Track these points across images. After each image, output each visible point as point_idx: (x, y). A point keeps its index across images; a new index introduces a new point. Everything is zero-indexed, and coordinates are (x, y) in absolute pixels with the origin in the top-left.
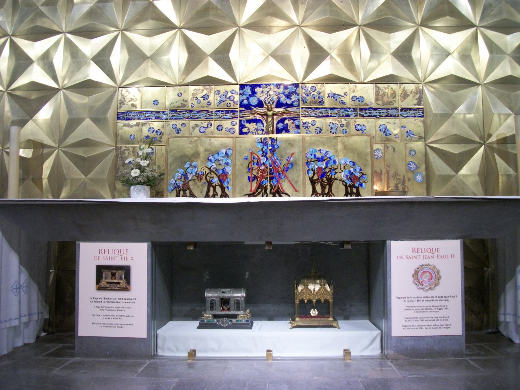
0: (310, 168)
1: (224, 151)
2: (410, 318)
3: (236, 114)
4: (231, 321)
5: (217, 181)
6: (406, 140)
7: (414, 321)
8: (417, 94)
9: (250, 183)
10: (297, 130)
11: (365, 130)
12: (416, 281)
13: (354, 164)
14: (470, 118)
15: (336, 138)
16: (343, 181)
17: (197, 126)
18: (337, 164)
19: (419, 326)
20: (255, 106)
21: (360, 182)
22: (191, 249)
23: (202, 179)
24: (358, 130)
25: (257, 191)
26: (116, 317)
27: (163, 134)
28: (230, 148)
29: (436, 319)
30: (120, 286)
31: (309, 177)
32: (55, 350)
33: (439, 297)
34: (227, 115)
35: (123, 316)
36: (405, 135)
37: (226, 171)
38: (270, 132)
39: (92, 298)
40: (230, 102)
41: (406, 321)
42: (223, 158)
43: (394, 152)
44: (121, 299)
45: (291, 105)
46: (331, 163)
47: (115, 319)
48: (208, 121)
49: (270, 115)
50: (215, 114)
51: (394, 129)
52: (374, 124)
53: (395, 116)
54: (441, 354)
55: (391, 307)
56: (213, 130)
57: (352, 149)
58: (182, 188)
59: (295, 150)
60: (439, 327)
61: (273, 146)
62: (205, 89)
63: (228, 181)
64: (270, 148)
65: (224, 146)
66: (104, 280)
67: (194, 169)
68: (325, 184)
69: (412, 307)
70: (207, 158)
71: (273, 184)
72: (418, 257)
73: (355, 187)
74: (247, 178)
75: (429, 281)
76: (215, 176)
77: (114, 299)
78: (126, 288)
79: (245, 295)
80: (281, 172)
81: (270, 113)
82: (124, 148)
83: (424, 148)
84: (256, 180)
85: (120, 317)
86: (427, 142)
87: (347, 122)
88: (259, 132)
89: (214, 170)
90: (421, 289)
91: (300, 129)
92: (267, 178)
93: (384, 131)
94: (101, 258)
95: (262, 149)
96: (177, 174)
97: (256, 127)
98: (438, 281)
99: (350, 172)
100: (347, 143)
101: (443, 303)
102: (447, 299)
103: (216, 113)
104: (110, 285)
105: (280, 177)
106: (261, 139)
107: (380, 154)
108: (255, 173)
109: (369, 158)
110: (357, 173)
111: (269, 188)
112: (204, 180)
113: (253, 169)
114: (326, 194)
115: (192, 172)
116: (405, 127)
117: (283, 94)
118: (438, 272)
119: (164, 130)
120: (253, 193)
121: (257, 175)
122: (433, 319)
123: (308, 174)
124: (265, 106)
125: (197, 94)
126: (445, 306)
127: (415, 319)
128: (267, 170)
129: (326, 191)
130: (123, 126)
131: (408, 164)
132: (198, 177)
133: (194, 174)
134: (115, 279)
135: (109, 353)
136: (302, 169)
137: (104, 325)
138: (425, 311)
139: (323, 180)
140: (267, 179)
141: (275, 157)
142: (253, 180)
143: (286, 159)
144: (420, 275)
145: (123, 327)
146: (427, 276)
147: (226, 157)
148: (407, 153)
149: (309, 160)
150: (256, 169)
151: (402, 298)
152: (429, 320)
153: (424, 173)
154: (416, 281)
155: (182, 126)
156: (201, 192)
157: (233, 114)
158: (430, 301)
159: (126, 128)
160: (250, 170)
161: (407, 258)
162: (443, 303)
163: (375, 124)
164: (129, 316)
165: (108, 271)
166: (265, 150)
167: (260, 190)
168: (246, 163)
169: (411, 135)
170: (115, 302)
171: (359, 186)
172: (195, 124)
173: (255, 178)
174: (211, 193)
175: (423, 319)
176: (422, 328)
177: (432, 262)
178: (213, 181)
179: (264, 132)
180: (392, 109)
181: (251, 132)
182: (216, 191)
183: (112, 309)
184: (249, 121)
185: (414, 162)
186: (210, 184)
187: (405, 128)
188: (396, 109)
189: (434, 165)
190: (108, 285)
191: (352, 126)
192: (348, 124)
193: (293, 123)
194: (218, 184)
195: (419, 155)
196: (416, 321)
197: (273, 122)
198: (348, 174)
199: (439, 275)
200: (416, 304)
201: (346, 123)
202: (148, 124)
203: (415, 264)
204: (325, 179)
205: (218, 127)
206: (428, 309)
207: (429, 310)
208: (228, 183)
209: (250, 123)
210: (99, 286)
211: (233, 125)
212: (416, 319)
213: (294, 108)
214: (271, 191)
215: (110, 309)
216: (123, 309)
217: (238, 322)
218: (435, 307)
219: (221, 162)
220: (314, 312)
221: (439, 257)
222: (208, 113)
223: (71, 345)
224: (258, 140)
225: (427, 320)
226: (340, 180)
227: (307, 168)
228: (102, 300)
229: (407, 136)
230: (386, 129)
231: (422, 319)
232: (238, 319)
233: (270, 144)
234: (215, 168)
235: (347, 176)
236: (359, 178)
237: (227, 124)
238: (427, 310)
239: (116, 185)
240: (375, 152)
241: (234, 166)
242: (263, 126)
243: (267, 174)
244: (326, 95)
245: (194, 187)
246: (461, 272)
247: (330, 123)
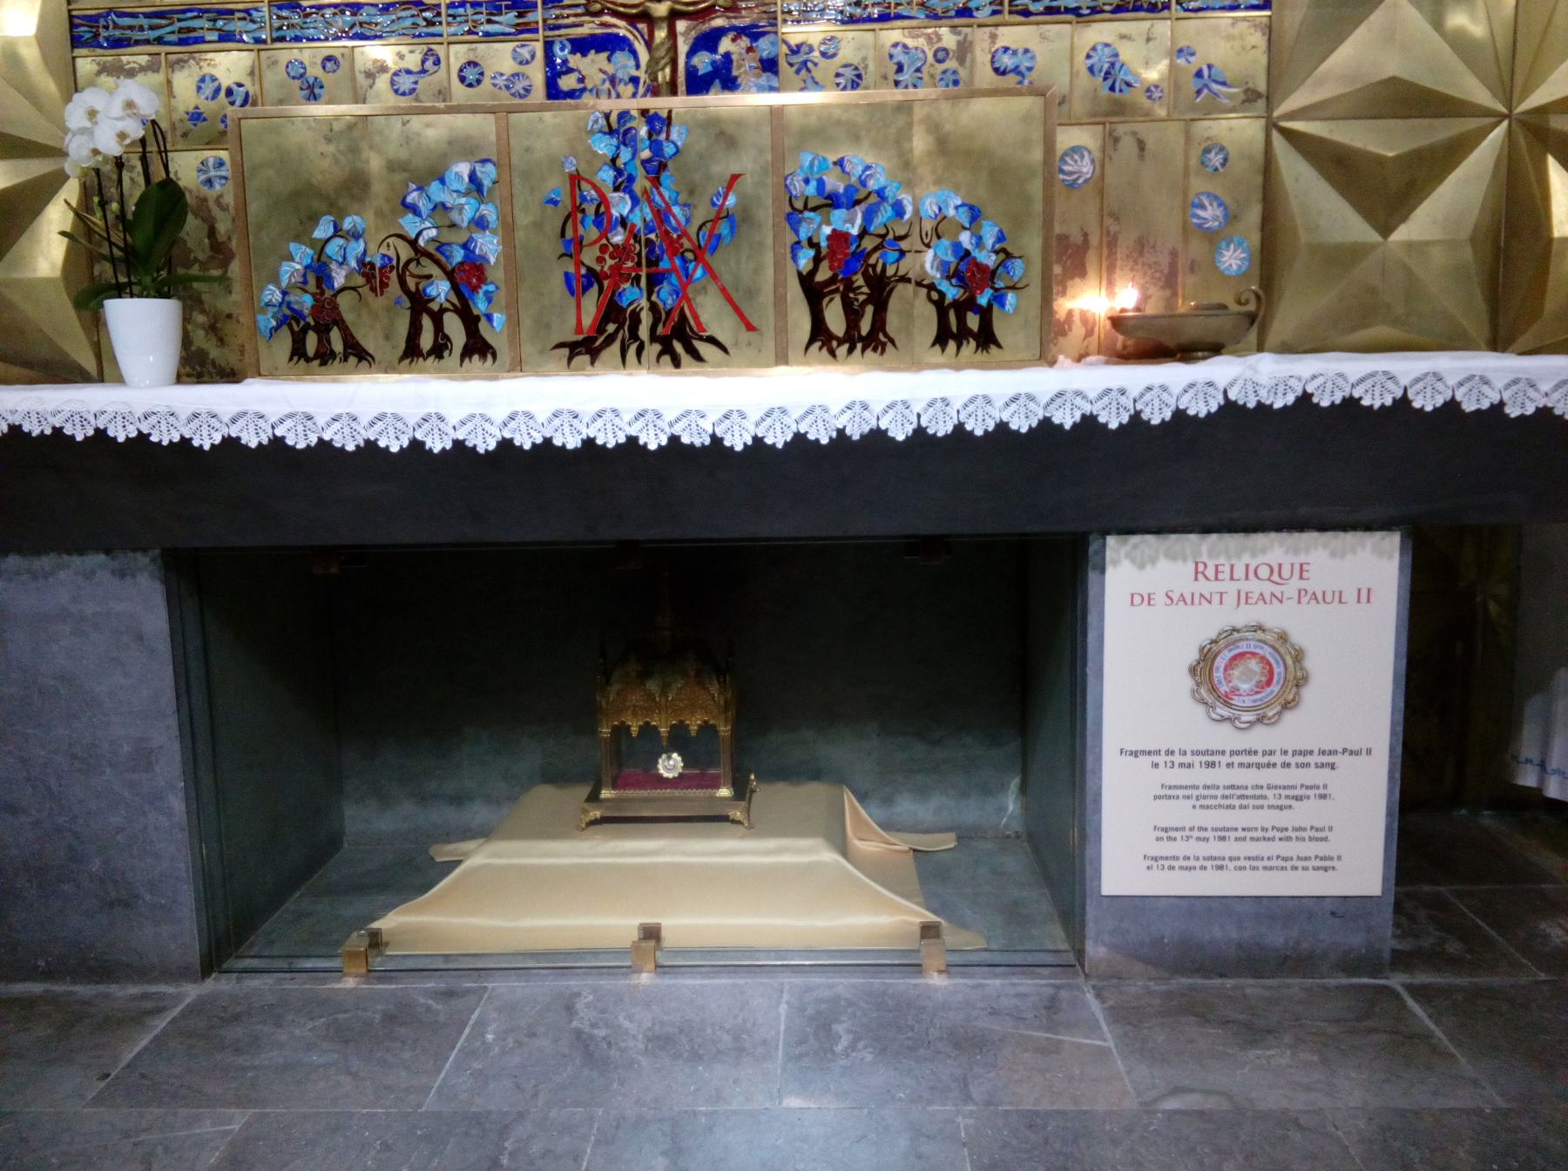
0: (804, 233)
1: (463, 169)
2: (1177, 829)
3: (530, 14)
5: (447, 294)
6: (1194, 108)
7: (1192, 841)
9: (572, 301)
10: (764, 79)
11: (1030, 69)
12: (1202, 691)
13: (975, 214)
15: (904, 108)
16: (931, 287)
18: (907, 217)
19: (1211, 858)
21: (996, 290)
23: (387, 285)
24: (1004, 73)
25: (600, 327)
28: (485, 157)
29: (1279, 835)
31: (800, 274)
33: (1295, 753)
34: (493, 18)
36: (1192, 85)
37: (477, 251)
38: (664, 89)
41: (1158, 839)
42: (463, 200)
43: (1141, 157)
46: (886, 213)
48: (425, 48)
49: (662, 19)
50: (450, 15)
51: (1147, 64)
52: (1067, 44)
54: (1295, 962)
55: (1100, 788)
56: (446, 84)
57: (968, 153)
58: (310, 320)
59: (744, 162)
60: (1289, 864)
61: (656, 147)
63: (487, 293)
64: (646, 154)
65: (463, 147)
67: (353, 244)
68: (862, 298)
69: (1186, 787)
70: (400, 200)
71: (661, 305)
72: (1216, 598)
73: (978, 309)
74: (558, 281)
75: (1257, 693)
80: (689, 256)
83: (1261, 137)
84: (596, 287)
86: (1276, 114)
87: (960, 38)
88: (621, 88)
89: (431, 249)
90: (1223, 719)
91: (776, 73)
92: (637, 280)
93: (1108, 73)
95: (614, 160)
96: (284, 263)
97: (610, 69)
98: (1297, 693)
99: (957, 246)
100: (948, 127)
101: (1312, 776)
103: (451, 12)
105: (687, 276)
107: (1086, 168)
108: (589, 257)
109: (1036, 187)
110: (984, 252)
111: (646, 319)
112: (394, 287)
113: (581, 242)
114: (861, 339)
115: (345, 258)
116: (1193, 54)
118: (1299, 656)
119: (257, 87)
120: (585, 339)
121: (598, 268)
122: (1267, 835)
123: (795, 258)
126: (1318, 787)
127: (1196, 834)
128: (637, 246)
129: (865, 326)
130: (99, 73)
131: (1194, 206)
132: (369, 277)
133: (353, 264)
135: (48, 963)
136: (769, 240)
138: (1237, 803)
139: (853, 283)
140: (638, 285)
141: (666, 194)
142: (586, 289)
143: (706, 200)
144: (1222, 669)
146: (1251, 670)
147: (475, 194)
148: (1193, 162)
149: (799, 205)
150: (596, 242)
151: (1144, 752)
152: (1252, 839)
153: (1255, 238)
154: (1202, 691)
155: (324, 67)
156: (387, 338)
157: (520, 15)
158: (1259, 766)
161: (1169, 602)
162: (1312, 776)
163: (1072, 43)
166: (625, 164)
167: (611, 328)
168: (555, 218)
169: (1215, 87)
171: (990, 305)
173: (593, 277)
175: (1227, 834)
176: (1220, 868)
177: (1273, 617)
179: (641, 90)
181: (591, 91)
182: (447, 330)
184: (582, 46)
185: (1216, 198)
187: (1192, 59)
191: (982, 56)
192: (964, 50)
193: (750, 50)
194: (453, 304)
195: (1238, 166)
196: (1198, 839)
197: (674, 47)
199: (1302, 669)
200: (1200, 776)
201: (959, 43)
202: (192, 62)
203: (1206, 624)
204: (859, 280)
206: (1247, 797)
207: (1252, 802)
208: (489, 300)
209: (584, 54)
211: (521, 63)
212: (1200, 833)
214: (653, 329)
218: (1277, 792)
219: (455, 216)
221: (1305, 600)
222: (422, 11)
224: (596, 121)
225: (1244, 839)
226: (919, 284)
227: (790, 238)
229: (1199, 92)
230: (1113, 64)
233: (642, 140)
234: (433, 240)
235: (943, 266)
236: (993, 273)
238: (1245, 802)
240: (1066, 163)
241: (508, 230)
242: (638, 66)
243: (639, 264)
245: (359, 315)
246: (1396, 656)
247: (895, 45)
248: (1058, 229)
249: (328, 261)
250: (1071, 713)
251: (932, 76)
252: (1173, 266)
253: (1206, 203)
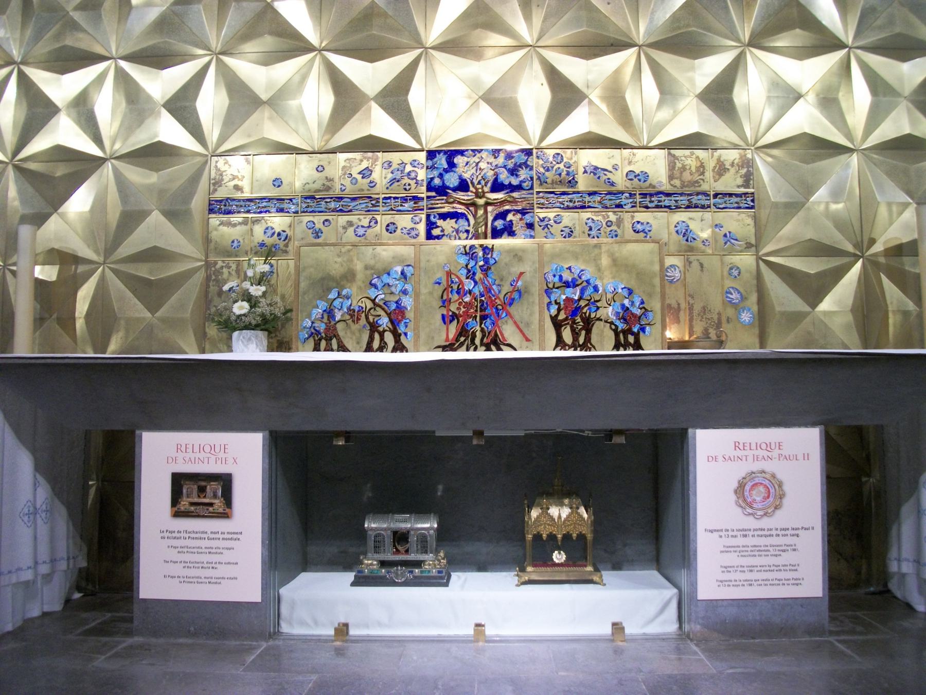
0: (553, 299)
1: (399, 269)
2: (731, 567)
3: (420, 203)
4: (411, 572)
5: (387, 323)
6: (724, 250)
7: (738, 572)
8: (743, 167)
9: (445, 327)
10: (528, 232)
11: (650, 231)
12: (740, 501)
13: (631, 292)
14: (837, 211)
15: (599, 246)
16: (612, 323)
17: (350, 224)
18: (600, 292)
19: (746, 581)
20: (455, 189)
21: (641, 325)
22: (340, 444)
23: (360, 319)
26: (206, 565)
27: (290, 240)
28: (409, 264)
29: (776, 568)
30: (214, 509)
31: (551, 316)
32: (99, 624)
33: (781, 530)
35: (219, 563)
36: (722, 240)
37: (402, 305)
38: (482, 236)
39: (163, 532)
41: (723, 572)
42: (397, 282)
43: (702, 270)
44: (215, 533)
45: (519, 188)
46: (590, 290)
47: (205, 568)
48: (371, 216)
49: (481, 206)
50: (383, 203)
51: (702, 230)
52: (666, 220)
53: (703, 207)
54: (786, 630)
55: (696, 548)
56: (379, 232)
57: (626, 266)
58: (323, 335)
59: (526, 267)
60: (781, 582)
61: (486, 261)
62: (365, 158)
63: (405, 323)
64: (482, 263)
65: (399, 260)
66: (184, 499)
67: (346, 301)
68: (580, 327)
69: (734, 547)
70: (369, 282)
71: (486, 329)
72: (744, 458)
73: (633, 334)
74: (439, 317)
75: (764, 501)
76: (382, 313)
77: (203, 532)
78: (225, 513)
79: (436, 526)
80: (500, 307)
81: (481, 202)
82: (220, 264)
83: (754, 264)
84: (456, 320)
85: (213, 565)
86: (760, 254)
87: (618, 217)
88: (461, 235)
89: (381, 303)
90: (750, 514)
91: (533, 229)
92: (476, 317)
93: (684, 234)
94: (180, 460)
95: (467, 266)
96: (314, 309)
97: (456, 226)
98: (781, 502)
99: (623, 306)
100: (617, 255)
101: (789, 540)
102: (796, 532)
103: (384, 201)
104: (195, 508)
105: (498, 316)
106: (465, 247)
107: (677, 274)
108: (453, 307)
109: (657, 281)
110: (635, 308)
111: (479, 335)
112: (363, 321)
113: (450, 301)
114: (580, 346)
115: (341, 307)
116: (722, 227)
117: (505, 167)
118: (780, 485)
119: (292, 232)
120: (450, 344)
121: (457, 312)
122: (771, 569)
123: (548, 309)
124: (472, 189)
125: (351, 167)
126: (792, 546)
127: (740, 569)
128: (476, 303)
129: (581, 340)
130: (220, 225)
131: (727, 293)
132: (352, 316)
133: (345, 310)
134: (205, 497)
135: (195, 629)
136: (537, 301)
137: (185, 579)
138: (757, 553)
139: (575, 320)
140: (476, 319)
141: (490, 280)
142: (451, 322)
143: (509, 283)
144: (748, 491)
145: (220, 583)
146: (760, 491)
147: (403, 280)
148: (726, 273)
149: (551, 286)
150: (457, 301)
151: (715, 531)
152: (764, 571)
153: (755, 308)
154: (740, 501)
155: (324, 224)
156: (358, 343)
157: (415, 203)
158: (766, 536)
159: (224, 229)
160: (445, 303)
161: (724, 460)
162: (789, 540)
163: (668, 221)
164: (229, 563)
165: (192, 483)
166: (472, 267)
167: (462, 339)
168: (439, 290)
169: (733, 241)
170: (205, 538)
171: (639, 332)
172: (348, 222)
173: (454, 316)
174: (376, 344)
175: (753, 569)
176: (751, 585)
177: (769, 466)
178: (380, 322)
179: (470, 236)
180: (698, 194)
181: (447, 236)
182: (385, 340)
183: (200, 550)
184: (444, 216)
185: (737, 289)
186: (374, 327)
188: (706, 194)
189: (772, 294)
190: (192, 508)
191: (627, 225)
192: (619, 222)
193: (521, 219)
194: (389, 328)
195: (745, 276)
196: (740, 571)
197: (486, 218)
198: (620, 310)
199: (782, 490)
200: (740, 541)
201: (617, 219)
202: (263, 221)
203: (739, 470)
204: (578, 319)
205: (388, 225)
206: (761, 551)
207: (763, 553)
208: (406, 326)
209: (445, 220)
210: (176, 509)
211: (415, 223)
212: (742, 569)
213: (524, 192)
214: (482, 340)
215: (195, 550)
216: (218, 551)
217: (424, 575)
218: (774, 548)
219: (393, 289)
221: (781, 459)
222: (371, 201)
223: (126, 614)
225: (761, 571)
226: (606, 322)
227: (547, 300)
228: (182, 535)
229: (726, 243)
230: (687, 230)
231: (751, 569)
232: (423, 569)
233: (480, 257)
234: (382, 299)
235: (618, 313)
236: (640, 317)
237: (404, 221)
238: (761, 553)
239: (207, 330)
240: (668, 272)
241: (417, 295)
242: (469, 225)
243: (476, 311)
244: (581, 170)
245: (346, 333)
246: (822, 484)
247: (588, 219)
251: (605, 233)
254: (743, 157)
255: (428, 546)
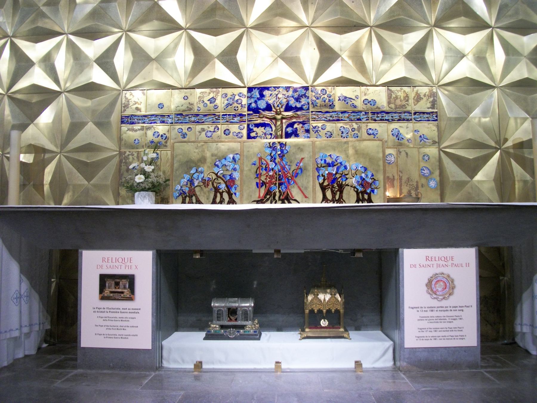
0: (321, 174)
1: (231, 156)
2: (424, 329)
3: (244, 118)
4: (239, 332)
5: (225, 187)
6: (420, 145)
7: (428, 332)
8: (431, 97)
9: (258, 189)
10: (306, 134)
11: (377, 134)
12: (429, 291)
13: (366, 169)
14: (485, 122)
15: (347, 143)
16: (355, 187)
17: (203, 130)
18: (348, 169)
19: (432, 337)
20: (264, 110)
21: (372, 188)
22: (197, 257)
23: (209, 185)
25: (265, 197)
26: (119, 328)
27: (168, 139)
28: (237, 153)
29: (450, 330)
30: (124, 295)
31: (319, 183)
32: (57, 362)
33: (453, 307)
35: (127, 326)
36: (419, 139)
37: (233, 177)
38: (279, 137)
39: (95, 308)
40: (238, 105)
41: (419, 332)
42: (230, 164)
43: (407, 157)
44: (125, 309)
45: (301, 109)
46: (342, 168)
47: (119, 329)
48: (215, 125)
49: (279, 119)
50: (222, 118)
51: (407, 133)
52: (386, 128)
53: (408, 120)
54: (456, 366)
55: (404, 318)
56: (220, 134)
57: (363, 154)
58: (187, 194)
59: (305, 155)
60: (453, 338)
61: (282, 151)
62: (212, 92)
63: (235, 187)
64: (279, 153)
65: (231, 151)
66: (107, 289)
67: (201, 174)
68: (336, 190)
69: (426, 317)
70: (214, 164)
71: (282, 191)
72: (431, 266)
73: (367, 193)
74: (255, 184)
75: (443, 291)
76: (222, 181)
77: (118, 309)
78: (130, 298)
80: (290, 178)
81: (279, 117)
82: (128, 153)
83: (437, 153)
84: (264, 186)
85: (124, 328)
86: (441, 147)
87: (358, 126)
88: (267, 136)
89: (221, 176)
90: (435, 298)
91: (309, 133)
92: (276, 184)
93: (397, 135)
94: (104, 267)
95: (271, 154)
96: (182, 179)
97: (264, 131)
98: (453, 291)
99: (361, 177)
100: (358, 148)
101: (458, 313)
102: (462, 309)
103: (223, 117)
104: (113, 294)
105: (289, 183)
106: (269, 143)
107: (393, 159)
108: (263, 178)
109: (381, 163)
110: (368, 179)
111: (278, 194)
112: (210, 186)
113: (261, 174)
114: (336, 200)
115: (198, 178)
116: (419, 132)
117: (293, 97)
118: (453, 281)
119: (169, 134)
120: (261, 200)
121: (265, 181)
122: (447, 330)
123: (318, 179)
124: (273, 109)
125: (203, 97)
126: (459, 316)
127: (429, 330)
128: (276, 175)
129: (337, 197)
130: (127, 130)
131: (422, 170)
132: (204, 183)
133: (200, 180)
134: (119, 288)
135: (113, 365)
136: (311, 175)
137: (107, 336)
138: (439, 321)
139: (334, 186)
140: (276, 185)
141: (284, 163)
142: (261, 186)
143: (295, 164)
144: (434, 285)
145: (127, 338)
146: (441, 285)
147: (234, 162)
148: (421, 158)
149: (319, 166)
150: (265, 174)
151: (415, 308)
152: (443, 331)
153: (438, 179)
154: (429, 291)
155: (188, 130)
156: (208, 199)
157: (241, 118)
158: (444, 311)
159: (130, 133)
160: (258, 176)
161: (420, 267)
162: (458, 313)
163: (387, 128)
164: (133, 327)
165: (112, 280)
166: (274, 155)
167: (268, 197)
168: (254, 168)
169: (425, 140)
170: (119, 312)
171: (370, 193)
172: (202, 128)
173: (263, 183)
174: (218, 200)
175: (436, 330)
176: (435, 339)
177: (446, 270)
178: (220, 187)
179: (273, 137)
180: (405, 112)
181: (259, 137)
182: (223, 197)
183: (116, 319)
184: (257, 125)
185: (427, 168)
186: (217, 190)
187: (418, 133)
188: (409, 112)
189: (448, 170)
190: (112, 295)
191: (364, 130)
192: (359, 129)
193: (302, 127)
194: (226, 190)
195: (432, 160)
196: (429, 331)
197: (282, 126)
198: (359, 180)
199: (454, 284)
200: (429, 314)
201: (358, 127)
202: (152, 128)
203: (429, 273)
204: (335, 185)
205: (225, 131)
206: (441, 319)
207: (443, 321)
208: (236, 189)
209: (258, 127)
210: (102, 295)
211: (241, 130)
212: (430, 330)
213: (304, 111)
214: (279, 197)
215: (113, 319)
216: (127, 319)
218: (449, 318)
219: (228, 168)
220: (324, 323)
221: (453, 266)
222: (215, 116)
223: (73, 356)
225: (441, 331)
226: (351, 186)
227: (317, 174)
228: (106, 310)
229: (421, 141)
230: (398, 133)
231: (436, 330)
232: (245, 330)
233: (278, 149)
234: (222, 174)
235: (358, 182)
236: (371, 184)
237: (234, 128)
238: (441, 321)
239: (120, 191)
240: (387, 158)
241: (242, 171)
242: (272, 131)
243: (276, 180)
244: (337, 99)
245: (201, 193)
246: (476, 281)
247: (341, 127)
248: (387, 175)
249: (193, 179)
250: (396, 295)
252: (417, 185)
253: (425, 169)
254: (431, 91)
255: (248, 317)
